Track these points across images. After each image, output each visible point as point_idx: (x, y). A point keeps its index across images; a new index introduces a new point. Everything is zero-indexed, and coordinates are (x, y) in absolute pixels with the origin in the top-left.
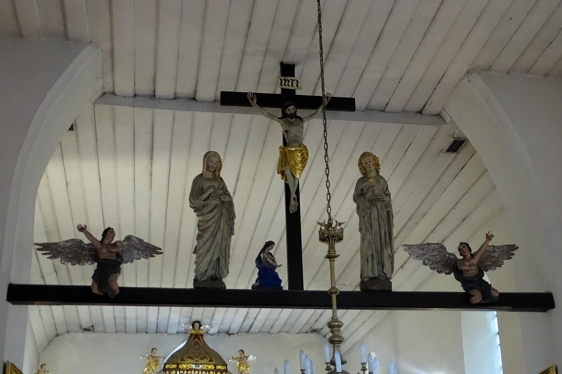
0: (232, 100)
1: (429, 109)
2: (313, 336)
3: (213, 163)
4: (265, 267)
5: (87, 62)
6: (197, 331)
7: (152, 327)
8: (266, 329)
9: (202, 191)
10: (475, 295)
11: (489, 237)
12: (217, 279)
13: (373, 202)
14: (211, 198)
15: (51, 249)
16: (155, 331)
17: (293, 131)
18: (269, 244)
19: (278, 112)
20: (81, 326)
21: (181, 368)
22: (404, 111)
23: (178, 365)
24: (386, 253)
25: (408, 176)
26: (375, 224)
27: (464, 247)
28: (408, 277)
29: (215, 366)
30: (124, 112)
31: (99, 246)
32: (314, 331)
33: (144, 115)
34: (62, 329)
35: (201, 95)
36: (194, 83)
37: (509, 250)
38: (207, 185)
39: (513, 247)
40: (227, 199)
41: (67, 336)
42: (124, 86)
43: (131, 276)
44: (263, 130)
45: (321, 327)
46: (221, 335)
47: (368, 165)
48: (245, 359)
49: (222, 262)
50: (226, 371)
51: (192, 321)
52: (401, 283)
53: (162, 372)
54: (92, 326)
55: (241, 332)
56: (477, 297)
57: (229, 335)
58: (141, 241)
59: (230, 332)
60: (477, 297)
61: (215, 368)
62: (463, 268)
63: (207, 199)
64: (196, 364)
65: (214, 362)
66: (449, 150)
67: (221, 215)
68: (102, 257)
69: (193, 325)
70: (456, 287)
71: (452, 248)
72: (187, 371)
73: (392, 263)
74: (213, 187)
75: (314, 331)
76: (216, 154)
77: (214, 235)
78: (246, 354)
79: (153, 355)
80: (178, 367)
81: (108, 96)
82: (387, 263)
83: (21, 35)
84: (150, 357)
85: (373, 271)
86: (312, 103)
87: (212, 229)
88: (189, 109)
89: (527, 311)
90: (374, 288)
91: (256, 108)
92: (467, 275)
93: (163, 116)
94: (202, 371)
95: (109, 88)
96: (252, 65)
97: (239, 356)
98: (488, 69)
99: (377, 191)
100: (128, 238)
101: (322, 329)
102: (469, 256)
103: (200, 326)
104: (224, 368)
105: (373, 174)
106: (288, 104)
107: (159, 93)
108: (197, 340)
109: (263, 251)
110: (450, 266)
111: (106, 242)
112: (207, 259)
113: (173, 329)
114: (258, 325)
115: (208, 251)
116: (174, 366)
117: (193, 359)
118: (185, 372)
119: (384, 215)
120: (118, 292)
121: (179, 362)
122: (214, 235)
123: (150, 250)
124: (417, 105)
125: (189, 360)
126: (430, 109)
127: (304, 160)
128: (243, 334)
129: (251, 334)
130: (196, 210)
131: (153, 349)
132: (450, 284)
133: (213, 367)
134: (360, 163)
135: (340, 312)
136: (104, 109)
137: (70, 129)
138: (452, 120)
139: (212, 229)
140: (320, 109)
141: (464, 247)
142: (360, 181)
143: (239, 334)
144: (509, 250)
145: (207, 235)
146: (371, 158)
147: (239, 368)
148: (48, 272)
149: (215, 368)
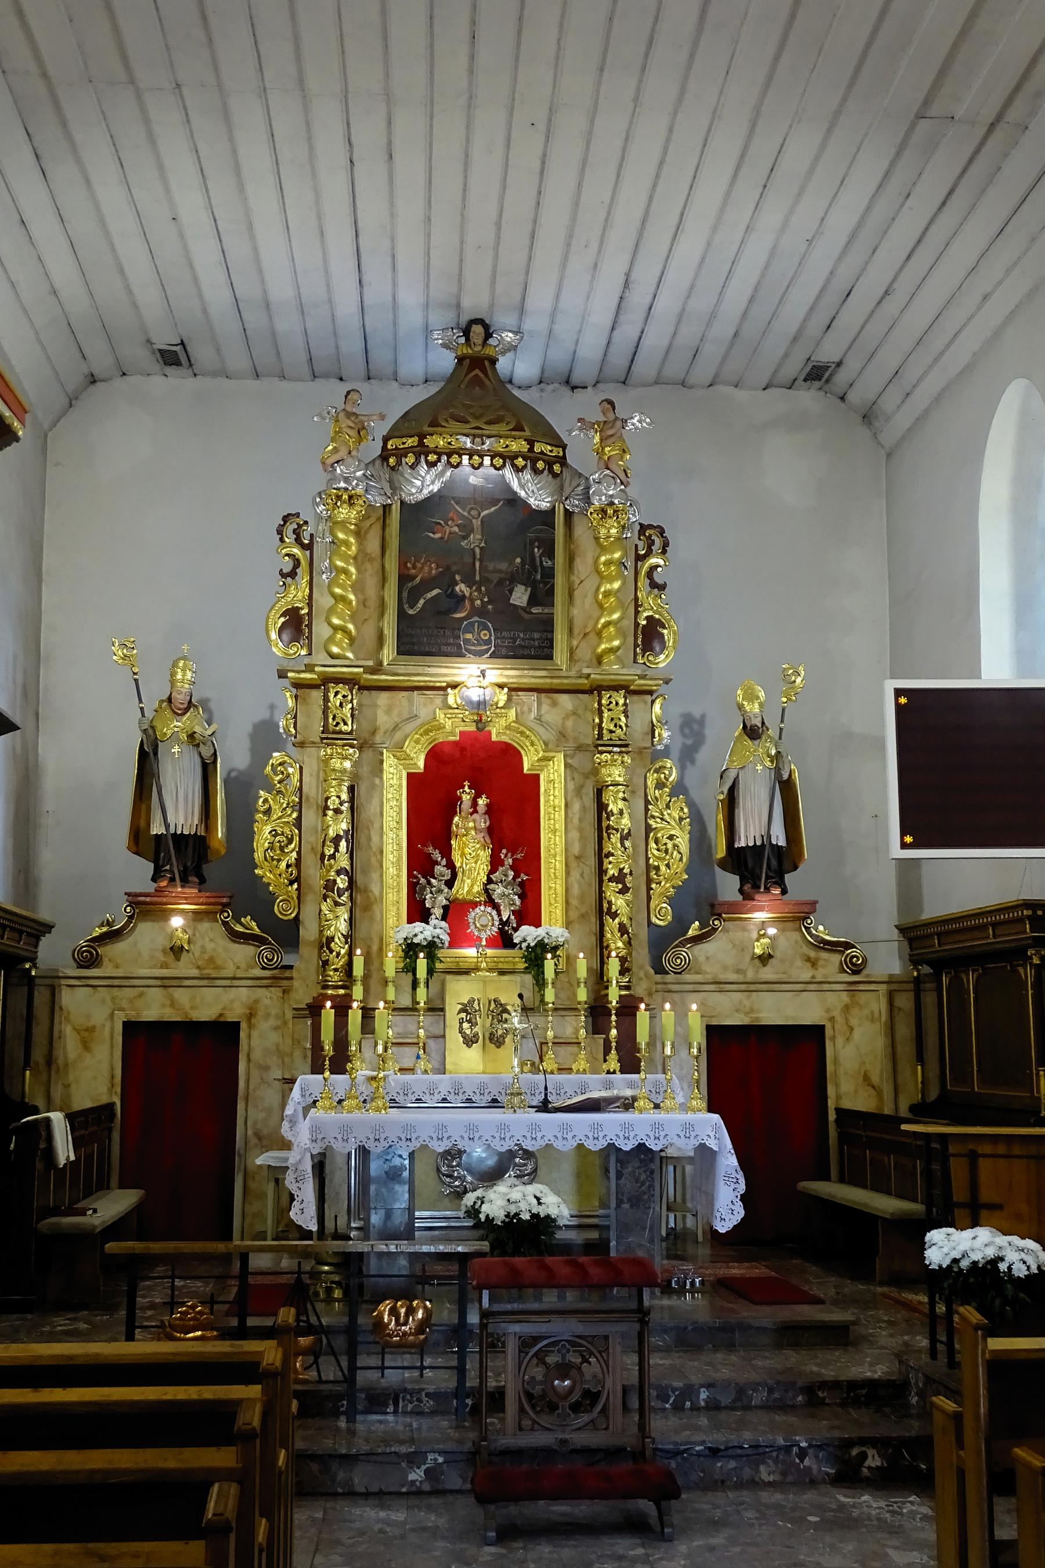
2: (808, 398)
6: (479, 348)
8: (674, 369)
16: (362, 372)
20: (149, 341)
21: (432, 446)
23: (422, 437)
29: (531, 443)
34: (101, 360)
41: (118, 383)
45: (837, 360)
46: (551, 387)
48: (619, 424)
50: (562, 461)
51: (464, 319)
53: (378, 462)
54: (182, 343)
55: (606, 381)
57: (573, 388)
59: (575, 379)
61: (531, 450)
64: (474, 436)
65: (527, 433)
69: (466, 332)
72: (449, 455)
78: (620, 413)
79: (349, 409)
80: (421, 443)
84: (342, 415)
89: (28, 1473)
94: (492, 458)
97: (602, 419)
101: (839, 364)
103: (488, 335)
104: (557, 452)
108: (477, 371)
116: (411, 442)
117: (467, 422)
118: (444, 458)
121: (427, 429)
125: (455, 426)
128: (612, 385)
129: (635, 386)
131: (348, 393)
133: (524, 447)
143: (600, 385)
147: (600, 452)
149: (531, 450)
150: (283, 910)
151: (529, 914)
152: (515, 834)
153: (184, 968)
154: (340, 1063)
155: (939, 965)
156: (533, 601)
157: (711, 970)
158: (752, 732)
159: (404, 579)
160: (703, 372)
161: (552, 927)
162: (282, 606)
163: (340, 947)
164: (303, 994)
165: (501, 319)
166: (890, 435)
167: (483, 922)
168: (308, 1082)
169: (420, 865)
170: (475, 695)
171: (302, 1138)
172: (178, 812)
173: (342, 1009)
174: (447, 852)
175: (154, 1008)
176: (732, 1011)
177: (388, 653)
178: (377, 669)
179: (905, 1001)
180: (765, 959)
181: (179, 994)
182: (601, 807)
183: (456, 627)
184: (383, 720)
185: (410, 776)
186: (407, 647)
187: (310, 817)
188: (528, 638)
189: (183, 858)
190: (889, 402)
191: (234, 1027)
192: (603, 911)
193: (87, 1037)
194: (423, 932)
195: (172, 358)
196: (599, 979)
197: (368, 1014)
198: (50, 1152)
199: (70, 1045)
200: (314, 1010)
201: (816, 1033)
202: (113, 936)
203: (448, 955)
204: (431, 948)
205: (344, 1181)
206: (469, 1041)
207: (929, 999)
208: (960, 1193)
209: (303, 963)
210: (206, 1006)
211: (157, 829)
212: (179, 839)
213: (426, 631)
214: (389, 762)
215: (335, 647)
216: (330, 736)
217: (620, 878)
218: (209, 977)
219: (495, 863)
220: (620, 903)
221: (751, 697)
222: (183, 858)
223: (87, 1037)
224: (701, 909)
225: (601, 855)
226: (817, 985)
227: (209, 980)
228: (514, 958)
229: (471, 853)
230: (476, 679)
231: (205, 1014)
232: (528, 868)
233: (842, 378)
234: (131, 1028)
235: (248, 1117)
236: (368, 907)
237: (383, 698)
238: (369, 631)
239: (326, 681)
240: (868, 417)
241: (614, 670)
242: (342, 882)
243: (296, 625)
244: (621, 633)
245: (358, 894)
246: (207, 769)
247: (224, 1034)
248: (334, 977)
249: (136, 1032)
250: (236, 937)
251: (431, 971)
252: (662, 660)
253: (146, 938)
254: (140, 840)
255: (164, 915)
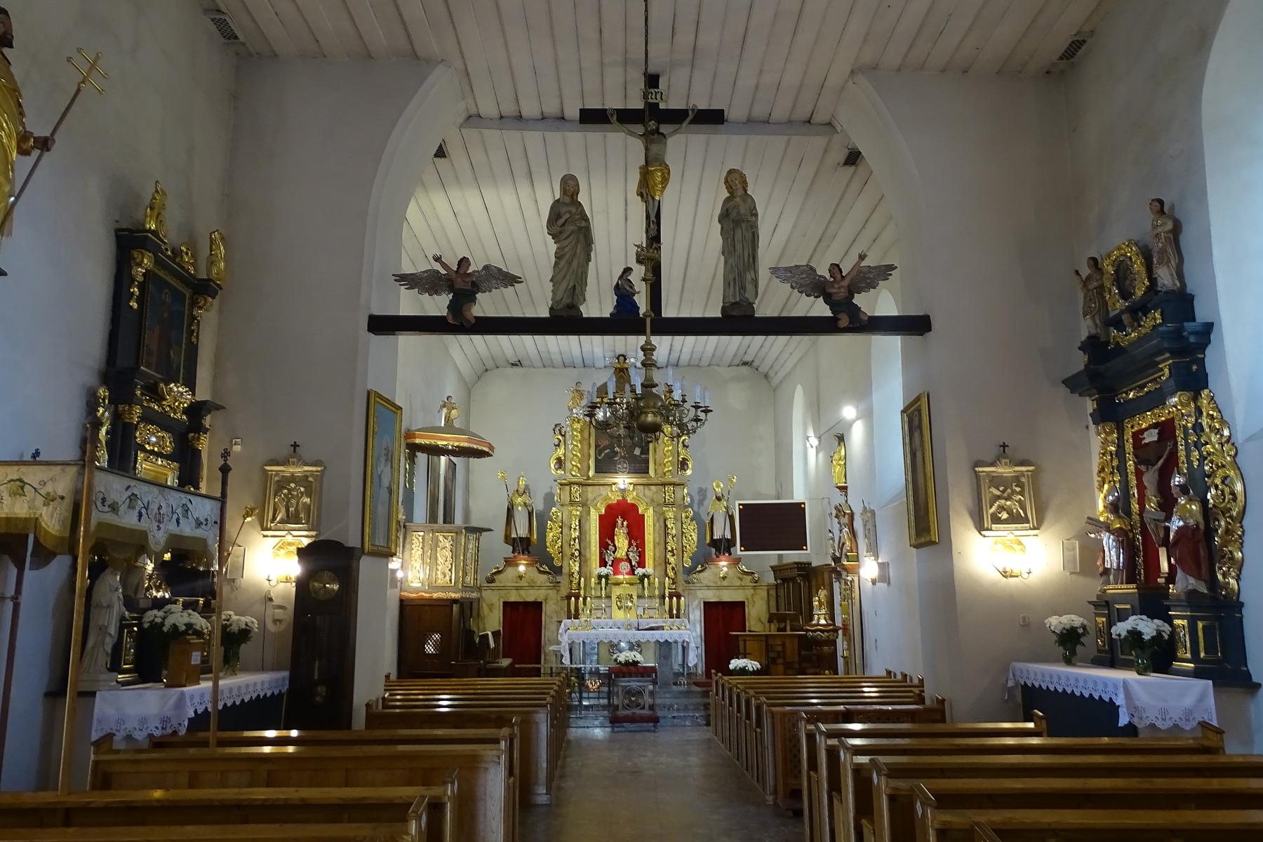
0: (592, 117)
1: (818, 118)
2: (744, 369)
3: (570, 187)
4: (624, 294)
5: (440, 84)
7: (578, 361)
9: (559, 216)
10: (846, 319)
11: (862, 257)
12: (573, 307)
13: (737, 223)
14: (569, 223)
15: (410, 281)
17: (655, 148)
18: (628, 270)
19: (640, 129)
22: (790, 122)
24: (749, 276)
25: (807, 194)
26: (739, 246)
27: (835, 268)
28: (774, 299)
30: (492, 135)
31: (454, 275)
32: (745, 364)
33: (513, 137)
34: (489, 364)
35: (568, 114)
36: (558, 101)
37: (885, 272)
38: (564, 209)
39: (891, 268)
40: (583, 224)
42: (488, 108)
43: (486, 305)
44: (626, 148)
47: (735, 183)
49: (578, 290)
52: (766, 308)
56: (844, 321)
58: (500, 270)
60: (844, 321)
62: (832, 290)
63: (563, 225)
66: (845, 164)
67: (578, 241)
68: (457, 286)
70: (826, 312)
71: (823, 271)
73: (756, 287)
74: (570, 212)
75: (745, 364)
76: (573, 178)
77: (570, 263)
81: (473, 119)
82: (749, 287)
83: (370, 57)
85: (734, 296)
86: (676, 117)
87: (567, 256)
88: (558, 129)
90: (734, 313)
91: (616, 125)
92: (835, 298)
93: (534, 138)
95: (473, 111)
96: (614, 76)
98: (875, 67)
99: (743, 211)
100: (486, 268)
102: (839, 276)
105: (740, 192)
106: (652, 119)
107: (524, 114)
109: (621, 277)
110: (819, 288)
111: (462, 271)
112: (563, 286)
113: (600, 364)
114: (685, 358)
115: (564, 278)
119: (749, 236)
120: (473, 321)
122: (570, 263)
123: (511, 280)
124: (803, 112)
126: (820, 117)
127: (665, 180)
130: (555, 236)
132: (821, 309)
134: (726, 182)
135: (652, 338)
136: (471, 134)
137: (436, 155)
138: (842, 130)
139: (567, 256)
140: (684, 124)
141: (835, 268)
142: (727, 201)
144: (885, 272)
145: (563, 263)
146: (737, 176)
148: (410, 304)
150: (557, 563)
151: (642, 564)
152: (636, 534)
153: (523, 583)
154: (576, 617)
155: (784, 580)
156: (642, 453)
157: (705, 582)
158: (719, 499)
159: (597, 446)
160: (705, 362)
161: (649, 569)
162: (555, 456)
163: (576, 575)
164: (564, 592)
165: (629, 354)
166: (775, 381)
167: (624, 566)
168: (566, 622)
169: (604, 546)
170: (622, 487)
171: (565, 640)
172: (521, 530)
173: (577, 598)
174: (613, 541)
175: (513, 598)
176: (712, 596)
177: (591, 473)
178: (589, 478)
179: (773, 593)
180: (724, 578)
181: (522, 592)
182: (666, 526)
183: (615, 463)
184: (590, 496)
185: (600, 516)
186: (598, 470)
187: (565, 531)
188: (640, 467)
189: (522, 546)
190: (771, 374)
191: (541, 603)
192: (667, 562)
193: (491, 607)
194: (604, 571)
195: (517, 364)
196: (662, 584)
197: (585, 599)
198: (488, 644)
199: (485, 610)
200: (568, 598)
201: (742, 604)
202: (499, 572)
203: (613, 578)
204: (607, 577)
205: (579, 653)
206: (620, 608)
207: (781, 592)
208: (742, 651)
209: (563, 580)
210: (530, 596)
211: (514, 535)
212: (521, 539)
213: (605, 466)
214: (592, 510)
215: (574, 474)
216: (572, 503)
217: (672, 551)
218: (532, 586)
219: (630, 545)
220: (672, 560)
221: (718, 486)
222: (522, 546)
223: (491, 607)
224: (702, 561)
225: (666, 543)
226: (743, 587)
227: (532, 587)
228: (635, 579)
229: (622, 541)
230: (623, 481)
231: (531, 599)
232: (641, 545)
233: (755, 364)
234: (506, 604)
235: (546, 634)
236: (586, 561)
237: (590, 488)
238: (585, 464)
239: (570, 484)
240: (766, 376)
241: (669, 478)
242: (577, 553)
243: (560, 463)
244: (672, 465)
245: (582, 557)
246: (530, 514)
247: (537, 606)
248: (574, 586)
249: (507, 605)
250: (540, 572)
251: (607, 584)
252: (689, 472)
253: (510, 572)
254: (507, 539)
255: (517, 565)
